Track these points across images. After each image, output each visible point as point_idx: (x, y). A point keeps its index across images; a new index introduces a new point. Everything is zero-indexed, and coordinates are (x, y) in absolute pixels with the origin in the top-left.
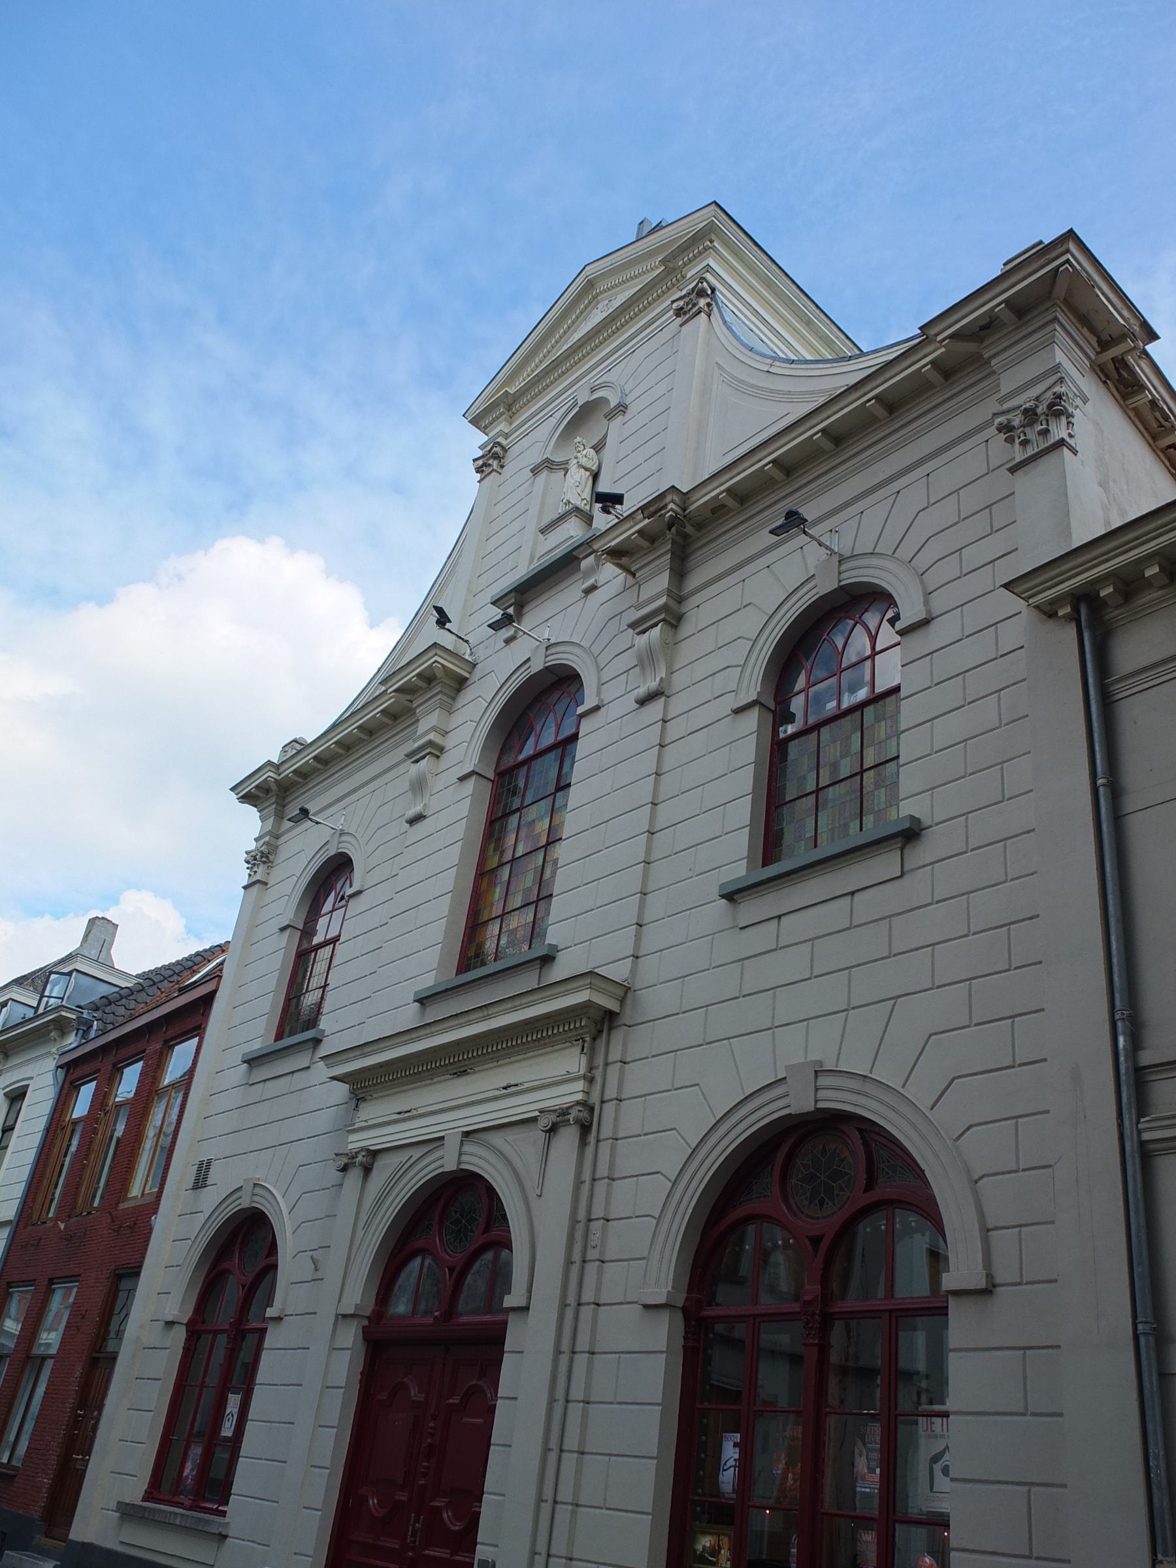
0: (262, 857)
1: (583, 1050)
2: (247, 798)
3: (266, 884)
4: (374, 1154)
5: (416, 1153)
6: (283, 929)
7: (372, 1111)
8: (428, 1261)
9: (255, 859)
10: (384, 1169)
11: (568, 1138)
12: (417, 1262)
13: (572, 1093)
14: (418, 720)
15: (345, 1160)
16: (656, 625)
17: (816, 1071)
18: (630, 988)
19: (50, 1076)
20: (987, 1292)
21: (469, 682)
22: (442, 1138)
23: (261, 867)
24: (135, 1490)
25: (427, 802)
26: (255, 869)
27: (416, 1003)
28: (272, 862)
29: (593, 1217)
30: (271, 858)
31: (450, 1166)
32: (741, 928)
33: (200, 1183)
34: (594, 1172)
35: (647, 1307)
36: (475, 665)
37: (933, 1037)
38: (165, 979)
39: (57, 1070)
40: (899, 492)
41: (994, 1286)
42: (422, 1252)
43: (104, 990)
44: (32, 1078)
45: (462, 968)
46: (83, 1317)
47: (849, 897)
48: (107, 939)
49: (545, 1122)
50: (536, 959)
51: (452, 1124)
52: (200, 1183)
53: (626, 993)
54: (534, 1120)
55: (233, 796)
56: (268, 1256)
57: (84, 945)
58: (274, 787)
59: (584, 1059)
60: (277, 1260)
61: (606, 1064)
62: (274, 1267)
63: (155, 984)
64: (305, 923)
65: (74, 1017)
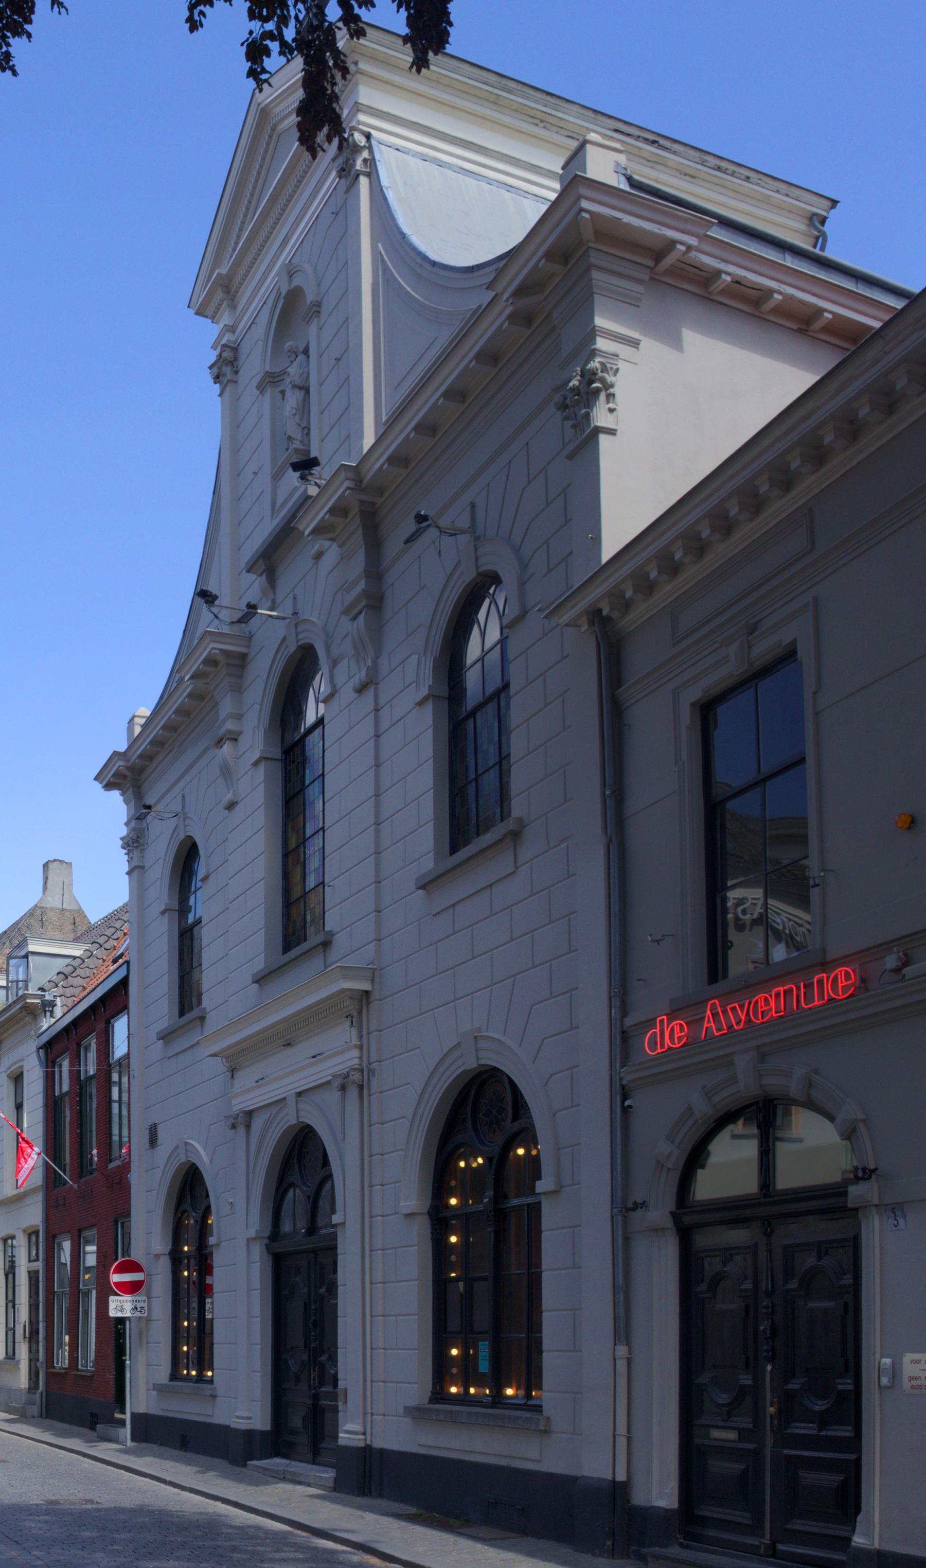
0: (133, 843)
1: (352, 1024)
2: (109, 786)
3: (143, 867)
4: (249, 1114)
5: (274, 1110)
6: (163, 913)
7: (247, 1077)
8: (298, 1191)
9: (129, 846)
10: (258, 1123)
11: (353, 1092)
12: (291, 1193)
13: (351, 1058)
14: (216, 704)
15: (231, 1120)
16: (360, 612)
17: (475, 1037)
18: (375, 969)
19: (35, 1056)
20: (555, 1192)
21: (250, 657)
22: (285, 1099)
23: (135, 851)
24: (163, 1373)
25: (235, 788)
26: (131, 855)
27: (255, 984)
28: (143, 845)
29: (374, 1153)
30: (141, 841)
31: (293, 1121)
32: (435, 915)
33: (153, 1141)
34: (370, 1121)
35: (407, 1215)
36: (250, 638)
37: (534, 1007)
38: (109, 938)
39: (38, 1052)
40: (510, 462)
41: (562, 1187)
42: (292, 1185)
43: (60, 964)
44: (23, 1060)
45: (287, 948)
46: (106, 1257)
47: (451, 911)
48: (65, 880)
49: (339, 1081)
50: (317, 946)
51: (286, 1087)
52: (153, 1141)
53: (374, 973)
54: (329, 1082)
55: (98, 786)
56: (515, 1118)
57: (46, 893)
58: (128, 773)
59: (354, 1031)
60: (331, 1170)
61: (369, 1033)
62: (330, 1176)
63: (101, 946)
64: (180, 904)
65: (39, 1001)
